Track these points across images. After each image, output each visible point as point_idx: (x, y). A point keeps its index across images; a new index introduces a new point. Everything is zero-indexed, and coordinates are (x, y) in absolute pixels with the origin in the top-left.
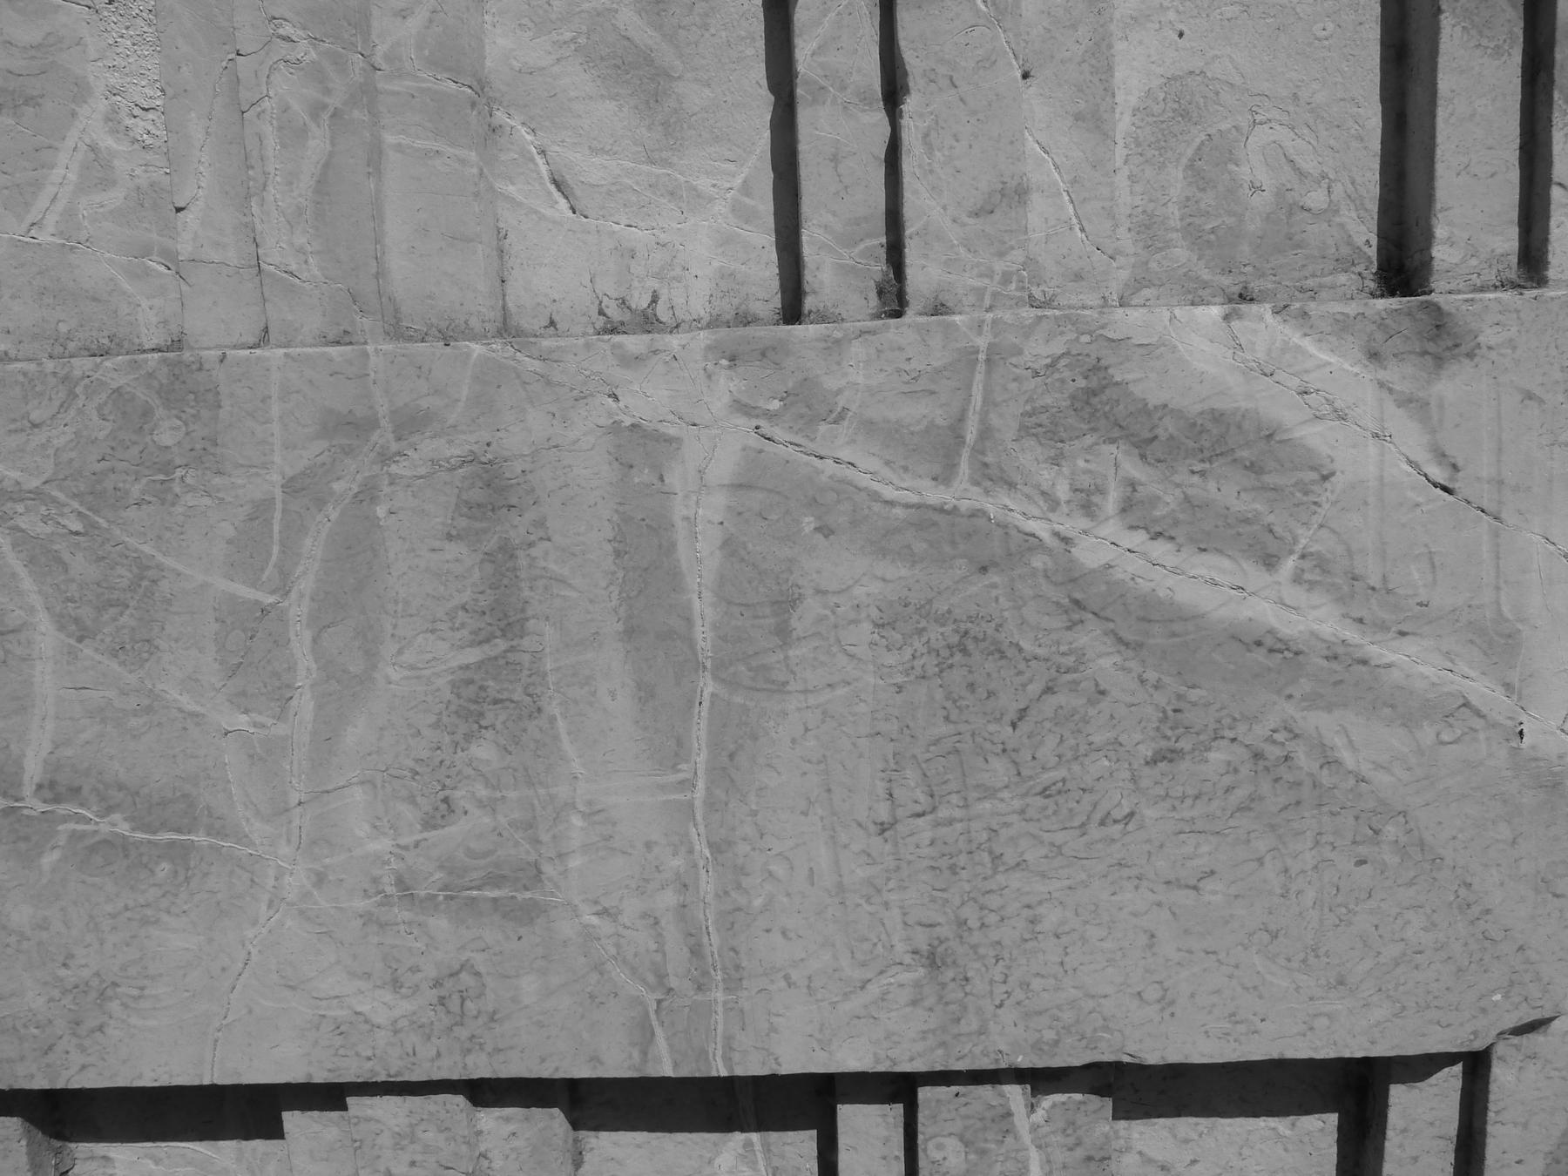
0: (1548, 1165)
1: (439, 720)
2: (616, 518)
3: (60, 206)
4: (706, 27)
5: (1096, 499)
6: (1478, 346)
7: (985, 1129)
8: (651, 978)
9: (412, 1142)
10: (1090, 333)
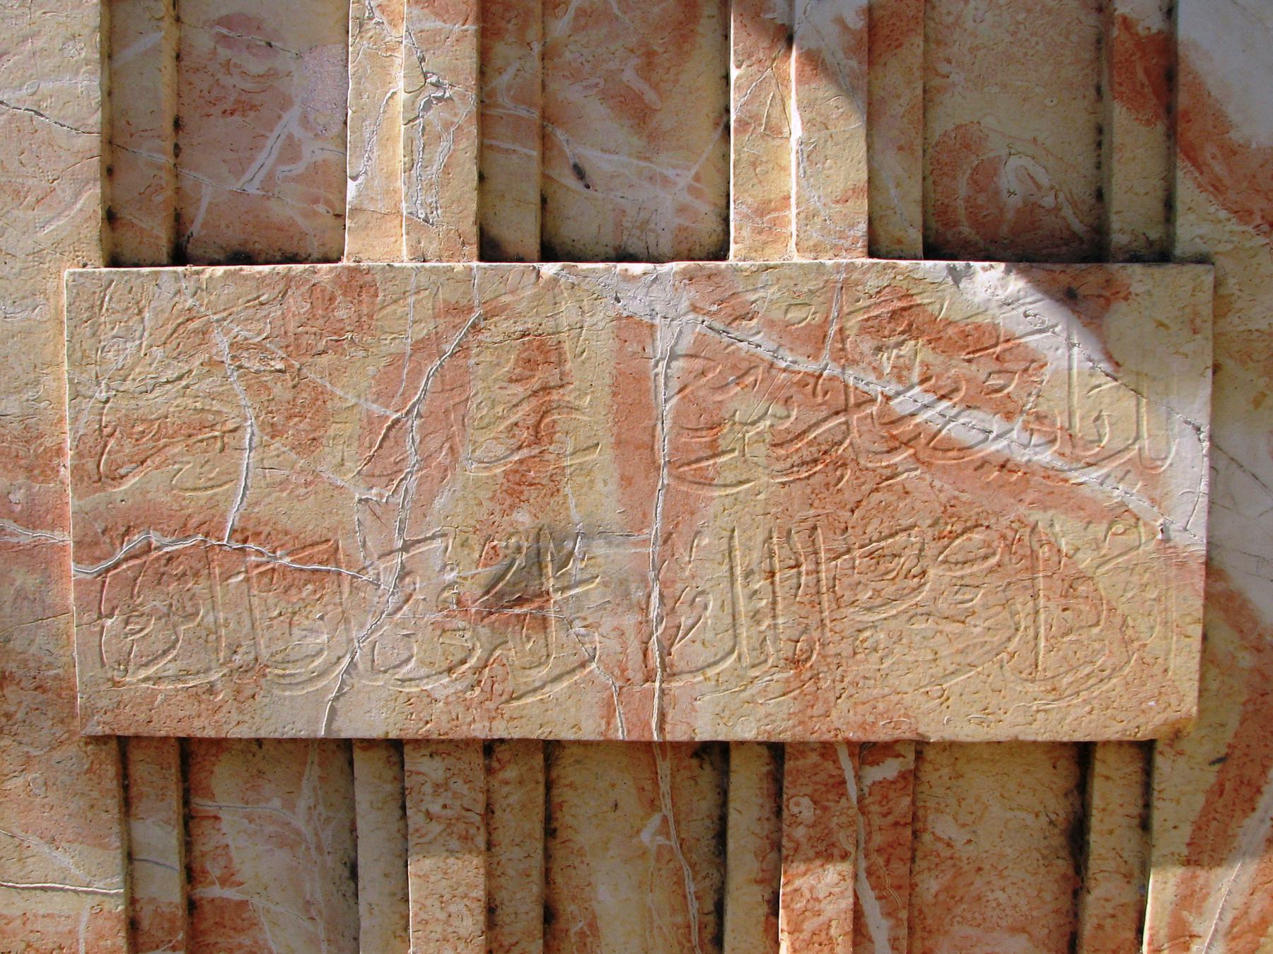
0: (1194, 831)
1: (494, 496)
2: (614, 372)
3: (264, 172)
4: (677, 81)
5: (905, 373)
6: (1130, 293)
7: (828, 792)
8: (617, 672)
9: (446, 790)
10: (903, 274)
